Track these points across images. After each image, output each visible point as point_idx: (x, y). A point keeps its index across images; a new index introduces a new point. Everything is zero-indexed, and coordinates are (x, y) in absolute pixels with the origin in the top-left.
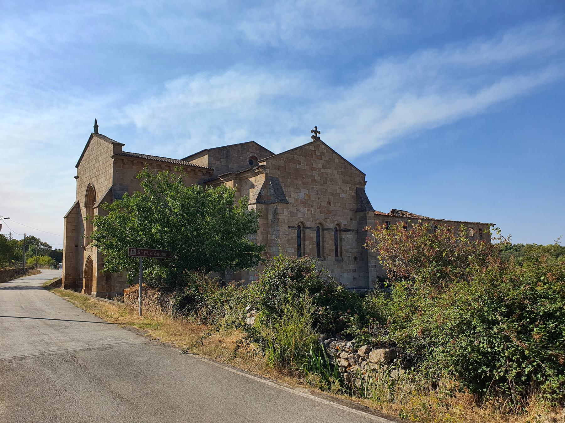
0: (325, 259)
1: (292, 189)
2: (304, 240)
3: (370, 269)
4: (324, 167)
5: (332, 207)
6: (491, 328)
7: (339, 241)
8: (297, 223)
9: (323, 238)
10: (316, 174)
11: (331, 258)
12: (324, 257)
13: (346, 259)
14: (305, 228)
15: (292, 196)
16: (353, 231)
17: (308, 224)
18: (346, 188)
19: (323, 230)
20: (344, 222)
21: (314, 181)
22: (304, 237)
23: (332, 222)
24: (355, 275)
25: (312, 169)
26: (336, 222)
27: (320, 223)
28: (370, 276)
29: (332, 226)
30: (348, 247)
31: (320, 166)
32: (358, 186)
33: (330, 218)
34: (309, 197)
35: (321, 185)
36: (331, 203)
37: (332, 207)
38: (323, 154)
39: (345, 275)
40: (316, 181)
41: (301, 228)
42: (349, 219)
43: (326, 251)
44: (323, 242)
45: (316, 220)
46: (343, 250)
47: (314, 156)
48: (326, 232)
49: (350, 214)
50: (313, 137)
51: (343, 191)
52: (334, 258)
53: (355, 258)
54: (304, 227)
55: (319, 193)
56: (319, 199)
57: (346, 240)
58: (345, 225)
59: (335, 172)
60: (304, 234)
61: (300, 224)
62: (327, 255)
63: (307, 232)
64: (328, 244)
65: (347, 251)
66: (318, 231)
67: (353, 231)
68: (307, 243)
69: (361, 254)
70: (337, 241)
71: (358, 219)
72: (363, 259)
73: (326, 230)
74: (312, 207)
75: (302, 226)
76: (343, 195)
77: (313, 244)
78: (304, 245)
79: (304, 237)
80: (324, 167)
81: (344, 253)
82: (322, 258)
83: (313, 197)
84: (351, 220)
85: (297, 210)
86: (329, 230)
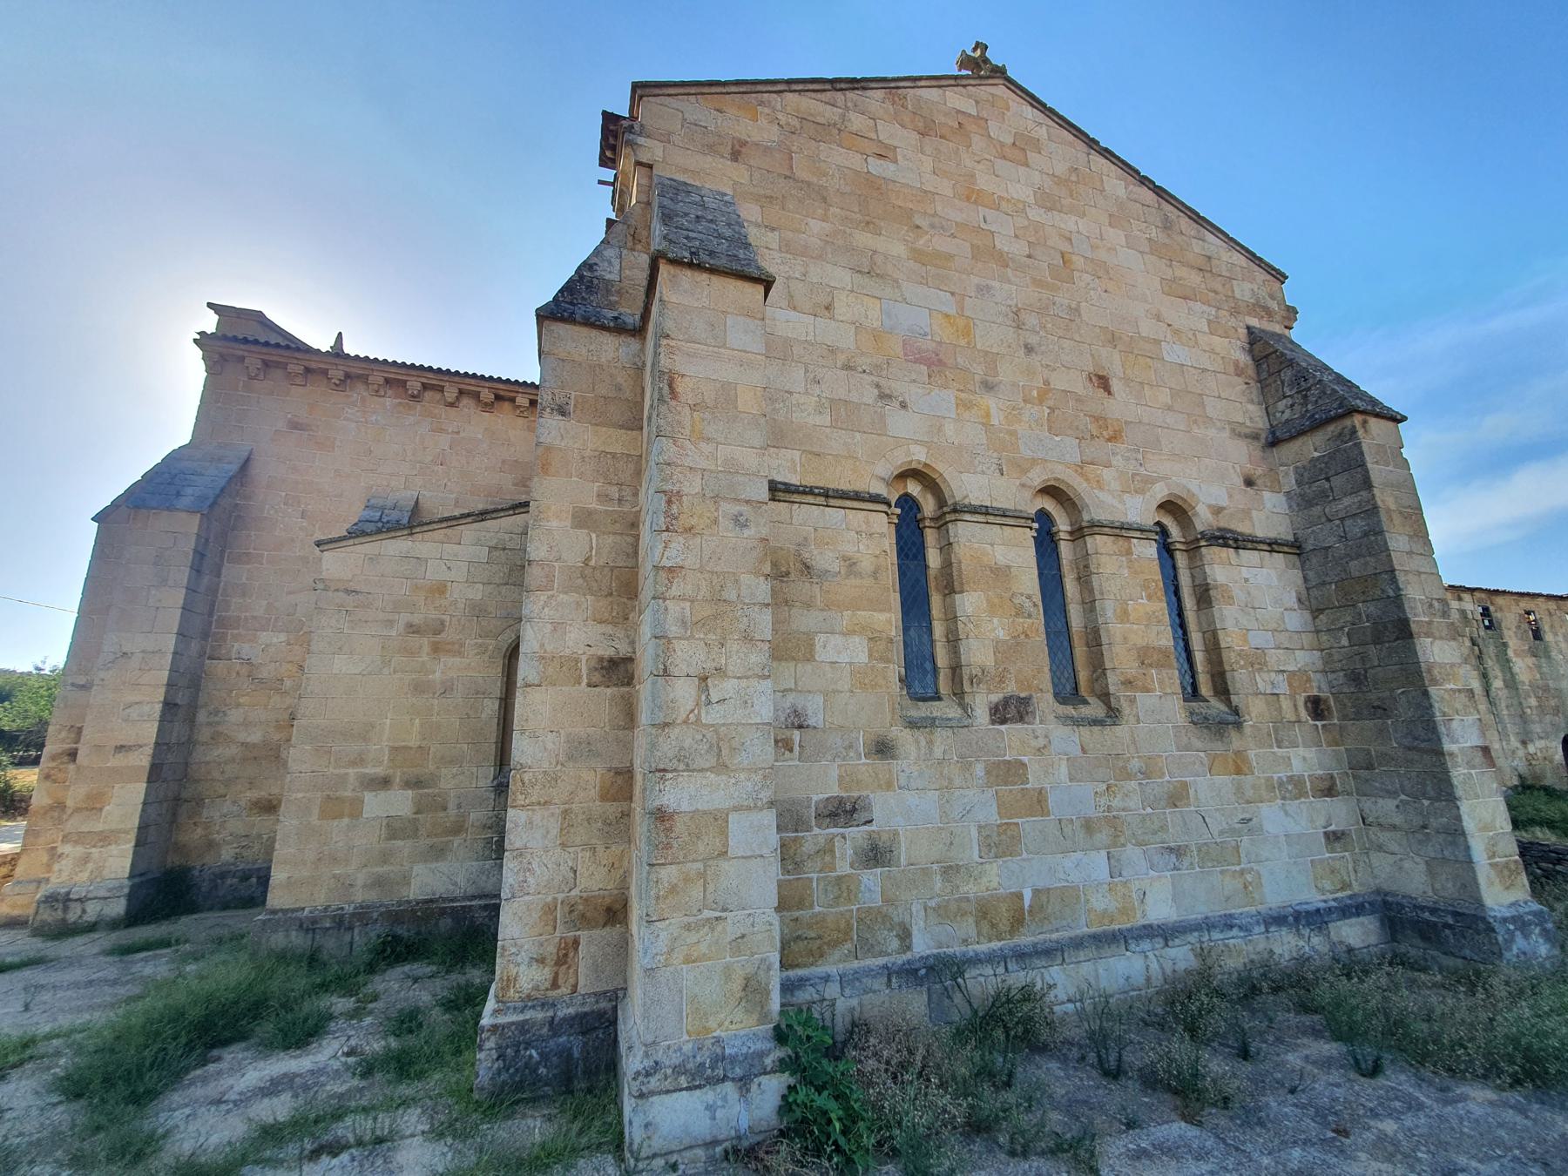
0: (1113, 714)
1: (840, 276)
2: (950, 588)
3: (1458, 774)
4: (1048, 202)
5: (1120, 405)
6: (89, 797)
7: (1189, 603)
8: (887, 469)
9: (1084, 579)
11: (1157, 708)
12: (1105, 697)
13: (1255, 711)
14: (951, 511)
15: (840, 309)
16: (1273, 546)
17: (968, 486)
18: (1194, 317)
19: (1078, 533)
20: (1213, 494)
22: (947, 565)
23: (1139, 484)
24: (1340, 813)
25: (973, 196)
26: (1160, 493)
27: (1051, 491)
28: (1469, 824)
29: (1140, 510)
30: (1258, 639)
32: (1254, 322)
33: (1117, 461)
34: (967, 332)
35: (1038, 283)
36: (1115, 385)
37: (1120, 405)
39: (1273, 817)
40: (1003, 260)
41: (918, 519)
42: (1239, 481)
43: (1121, 662)
44: (1090, 605)
45: (1022, 467)
46: (1229, 658)
47: (978, 142)
48: (1099, 544)
49: (1242, 456)
51: (1177, 332)
52: (1175, 709)
53: (1317, 707)
54: (941, 501)
55: (1031, 320)
56: (1029, 349)
57: (1237, 592)
58: (1217, 511)
59: (1115, 236)
60: (946, 547)
61: (914, 488)
62: (1128, 683)
63: (969, 538)
64: (1124, 616)
65: (1257, 661)
66: (1046, 542)
67: (1273, 546)
68: (969, 603)
69: (1356, 678)
70: (1187, 600)
71: (1290, 482)
72: (1380, 710)
73: (1096, 527)
74: (989, 387)
75: (928, 506)
76: (1175, 353)
77: (1019, 612)
78: (952, 618)
79: (947, 565)
81: (1239, 678)
82: (1095, 709)
83: (993, 336)
84: (1249, 483)
85: (884, 396)
86: (1121, 530)
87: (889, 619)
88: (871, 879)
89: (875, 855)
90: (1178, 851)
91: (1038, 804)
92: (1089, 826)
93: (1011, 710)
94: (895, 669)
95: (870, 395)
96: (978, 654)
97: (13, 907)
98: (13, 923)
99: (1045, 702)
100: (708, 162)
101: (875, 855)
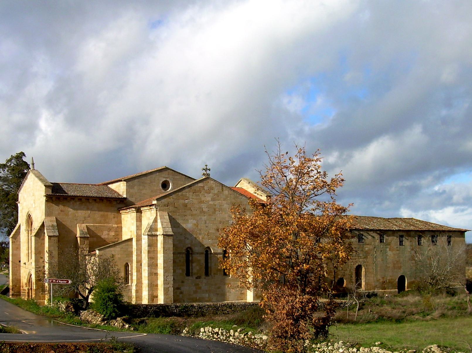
2: (192, 263)
4: (213, 199)
10: (204, 206)
21: (202, 212)
22: (192, 259)
31: (209, 199)
38: (212, 188)
40: (204, 212)
50: (204, 174)
55: (208, 222)
68: (194, 265)
80: (213, 199)
87: (185, 268)
88: (181, 295)
89: (181, 293)
90: (218, 294)
91: (200, 288)
92: (206, 291)
93: (199, 278)
94: (185, 273)
95: (183, 238)
96: (195, 271)
97: (133, 224)
98: (4, 166)
99: (203, 276)
100: (85, 333)
101: (181, 293)
